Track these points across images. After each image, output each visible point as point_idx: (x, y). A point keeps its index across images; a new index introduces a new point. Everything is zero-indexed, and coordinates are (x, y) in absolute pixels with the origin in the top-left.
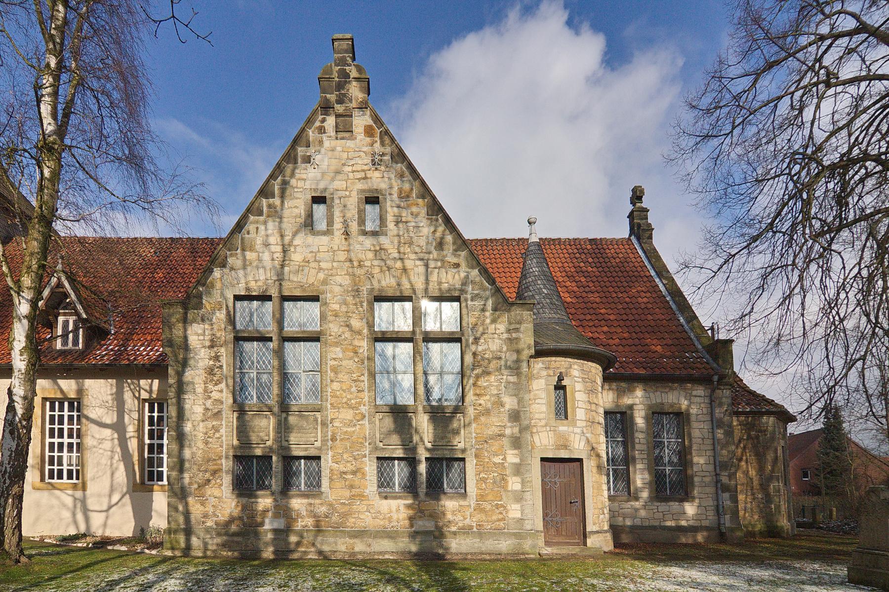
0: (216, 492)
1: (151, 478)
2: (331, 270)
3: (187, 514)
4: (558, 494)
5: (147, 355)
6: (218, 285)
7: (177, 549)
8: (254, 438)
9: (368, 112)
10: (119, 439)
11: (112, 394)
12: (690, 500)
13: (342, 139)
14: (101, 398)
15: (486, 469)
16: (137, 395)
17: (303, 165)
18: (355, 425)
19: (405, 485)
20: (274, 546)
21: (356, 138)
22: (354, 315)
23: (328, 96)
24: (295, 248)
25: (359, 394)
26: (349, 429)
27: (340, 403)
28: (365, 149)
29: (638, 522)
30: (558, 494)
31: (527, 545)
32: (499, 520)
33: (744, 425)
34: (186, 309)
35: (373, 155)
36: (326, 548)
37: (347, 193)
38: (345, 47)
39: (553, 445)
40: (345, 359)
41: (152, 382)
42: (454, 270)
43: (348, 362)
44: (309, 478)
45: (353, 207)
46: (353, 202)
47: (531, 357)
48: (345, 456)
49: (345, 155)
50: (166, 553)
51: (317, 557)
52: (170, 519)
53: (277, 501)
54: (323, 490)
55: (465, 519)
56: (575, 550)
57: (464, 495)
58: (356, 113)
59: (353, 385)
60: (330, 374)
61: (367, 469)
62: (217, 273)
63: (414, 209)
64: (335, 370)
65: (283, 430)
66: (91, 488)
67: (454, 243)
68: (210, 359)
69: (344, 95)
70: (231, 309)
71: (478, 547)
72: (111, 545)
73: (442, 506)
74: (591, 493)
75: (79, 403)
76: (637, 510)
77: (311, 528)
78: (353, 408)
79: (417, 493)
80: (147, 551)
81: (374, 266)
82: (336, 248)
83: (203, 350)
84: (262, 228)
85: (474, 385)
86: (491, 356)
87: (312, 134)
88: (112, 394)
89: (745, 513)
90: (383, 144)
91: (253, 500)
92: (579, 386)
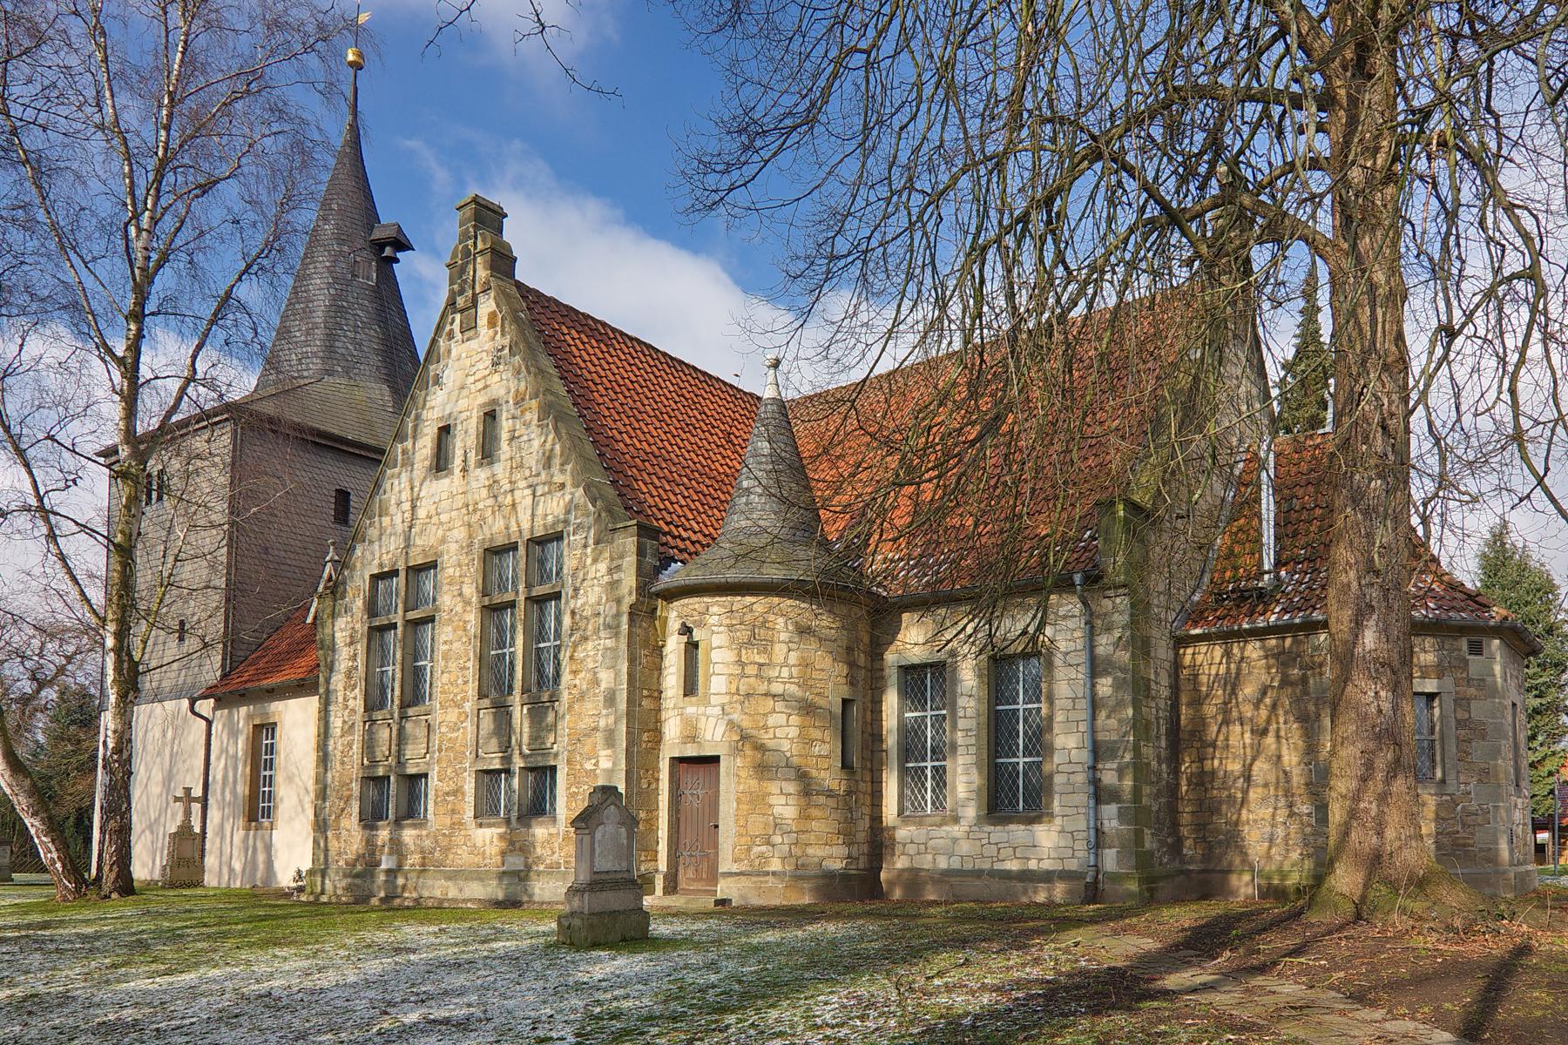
12: (1046, 819)
29: (956, 864)
33: (1273, 656)
55: (553, 853)
57: (554, 819)
76: (955, 840)
85: (571, 658)
89: (1270, 848)
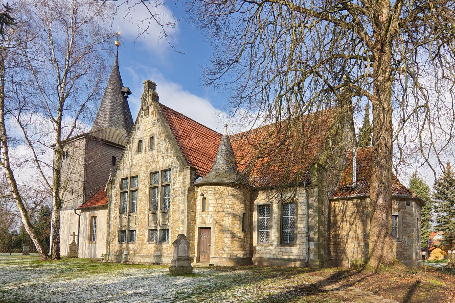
6: (118, 176)
12: (295, 245)
29: (272, 256)
76: (271, 250)
84: (128, 155)
85: (173, 201)
89: (353, 254)
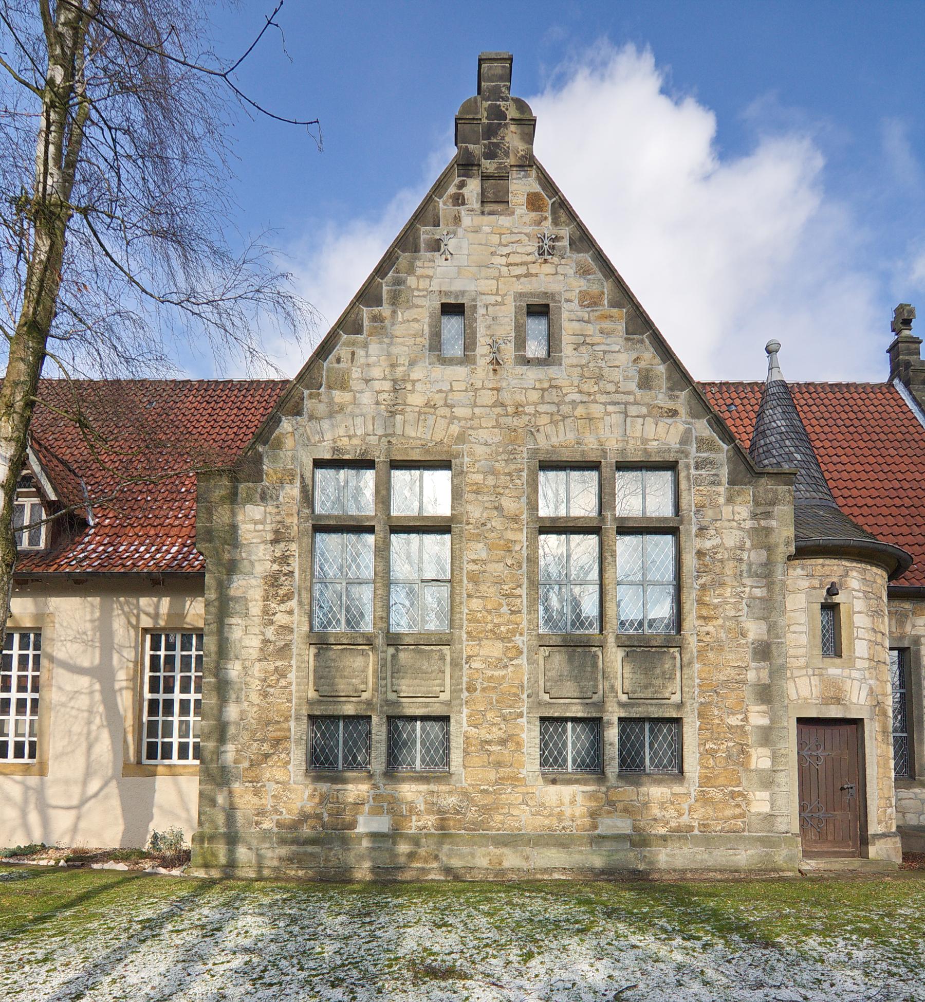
0: (280, 775)
1: (152, 755)
2: (471, 419)
3: (230, 813)
4: (822, 775)
5: (152, 558)
6: (289, 443)
7: (213, 867)
8: (342, 687)
9: (534, 173)
10: (102, 692)
11: (92, 621)
13: (492, 213)
14: (75, 628)
15: (716, 735)
16: (134, 621)
17: (429, 254)
18: (506, 667)
19: (583, 761)
20: (373, 859)
21: (513, 213)
22: (507, 491)
23: (471, 147)
24: (413, 385)
25: (513, 617)
26: (496, 673)
27: (481, 632)
28: (528, 230)
30: (822, 775)
31: (781, 856)
32: (735, 817)
34: (235, 480)
35: (541, 239)
36: (456, 863)
37: (499, 299)
38: (499, 71)
39: (817, 698)
40: (491, 562)
41: (159, 602)
42: (669, 421)
43: (496, 565)
44: (428, 751)
45: (508, 319)
46: (508, 313)
47: (790, 558)
48: (489, 716)
49: (495, 239)
50: (196, 874)
51: (442, 878)
52: (203, 818)
53: (378, 788)
54: (453, 769)
55: (681, 815)
56: (855, 863)
58: (514, 174)
59: (504, 602)
60: (467, 586)
61: (524, 736)
62: (286, 425)
63: (607, 325)
64: (474, 579)
65: (389, 674)
66: (54, 770)
67: (669, 378)
68: (274, 562)
69: (497, 145)
70: (309, 481)
71: (702, 860)
72: (97, 862)
73: (644, 795)
74: (875, 774)
75: (38, 636)
77: (433, 831)
78: (502, 639)
79: (603, 773)
80: (162, 870)
81: (540, 413)
82: (479, 384)
83: (262, 547)
84: (360, 353)
86: (726, 556)
87: (443, 206)
88: (92, 621)
90: (556, 222)
91: (339, 786)
92: (859, 605)
